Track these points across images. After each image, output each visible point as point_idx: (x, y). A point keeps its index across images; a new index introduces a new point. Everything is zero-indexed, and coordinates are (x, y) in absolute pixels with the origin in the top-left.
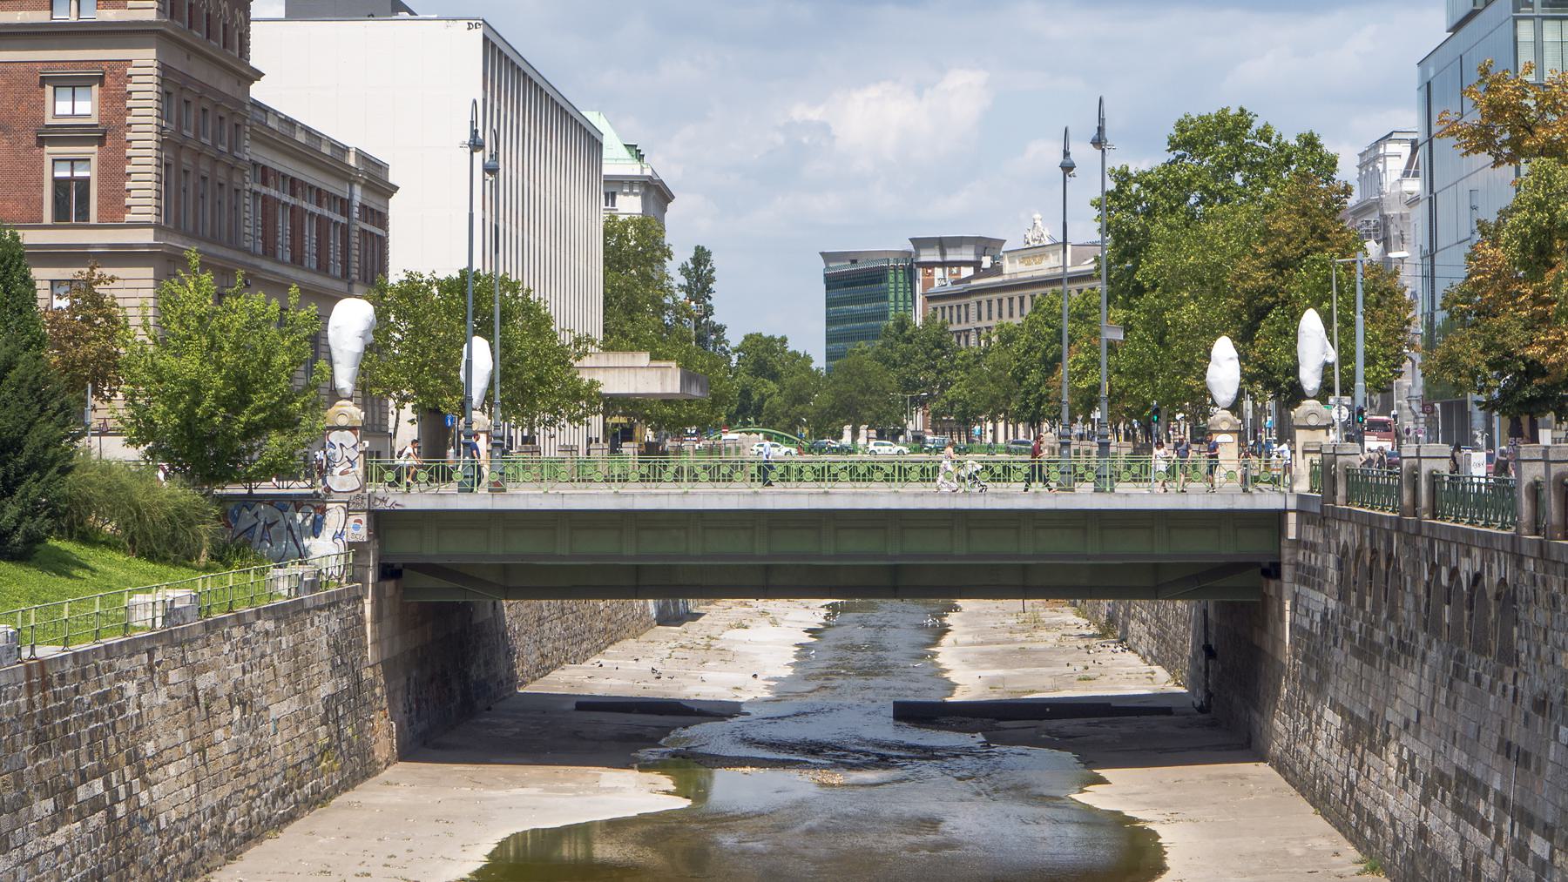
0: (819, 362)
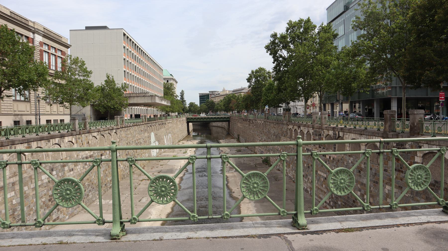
0: (199, 105)
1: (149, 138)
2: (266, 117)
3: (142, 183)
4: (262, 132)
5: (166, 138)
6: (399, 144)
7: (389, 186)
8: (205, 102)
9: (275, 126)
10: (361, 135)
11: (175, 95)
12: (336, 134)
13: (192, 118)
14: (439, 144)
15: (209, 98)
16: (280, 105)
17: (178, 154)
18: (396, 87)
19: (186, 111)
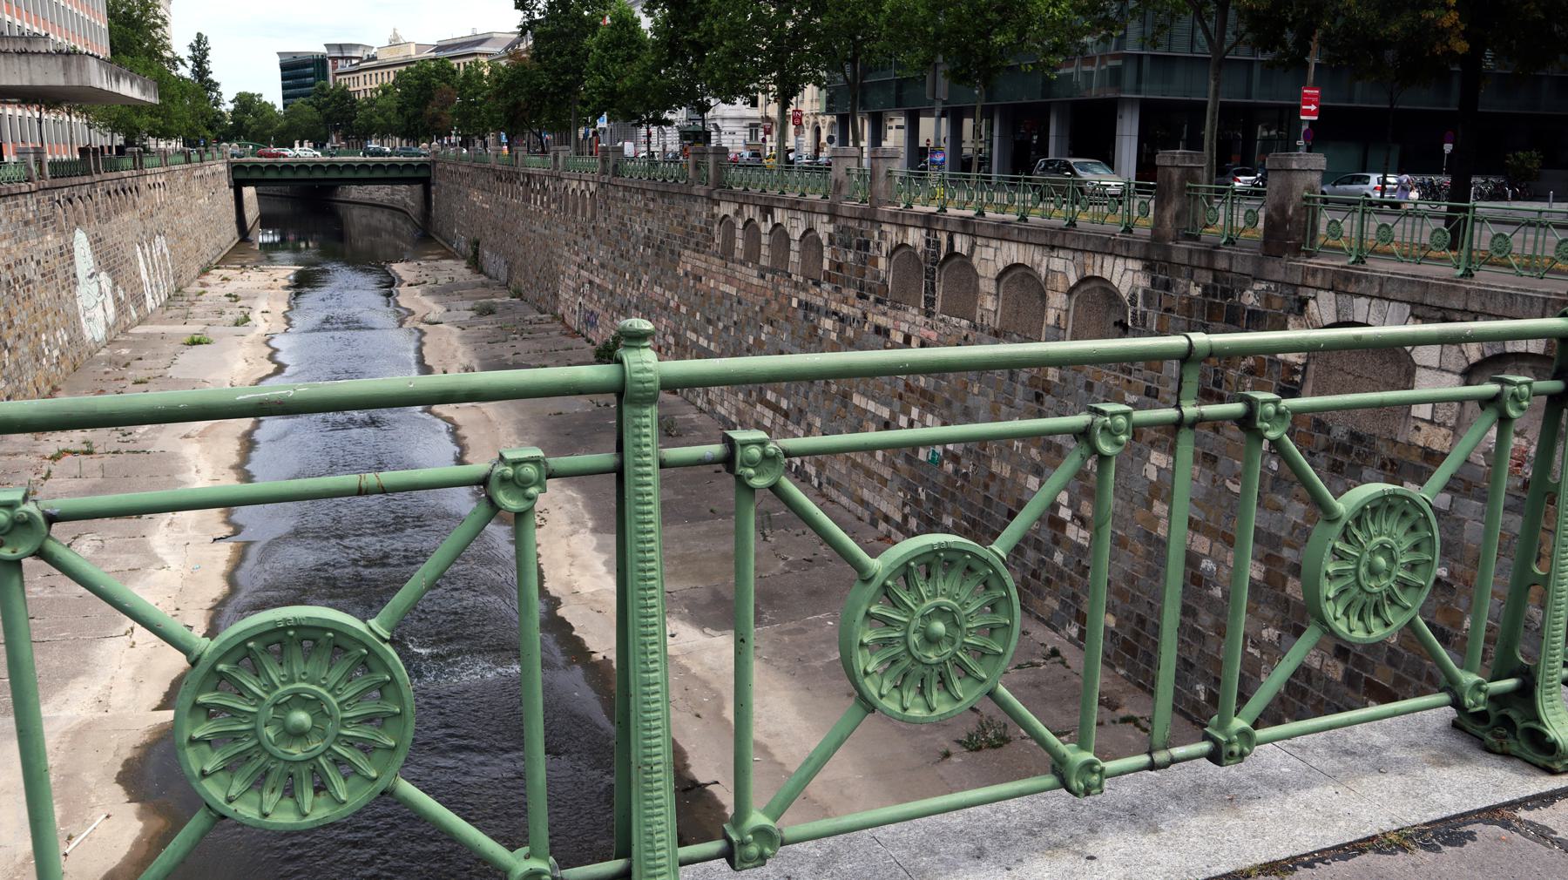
0: (279, 106)
1: (66, 256)
2: (611, 164)
3: (56, 467)
4: (590, 231)
5: (145, 256)
6: (1215, 288)
7: (1164, 452)
8: (308, 95)
9: (651, 206)
10: (1053, 248)
11: (167, 54)
12: (938, 244)
13: (255, 167)
14: (1380, 291)
15: (325, 77)
16: (667, 115)
17: (210, 329)
18: (1140, 57)
19: (222, 133)
